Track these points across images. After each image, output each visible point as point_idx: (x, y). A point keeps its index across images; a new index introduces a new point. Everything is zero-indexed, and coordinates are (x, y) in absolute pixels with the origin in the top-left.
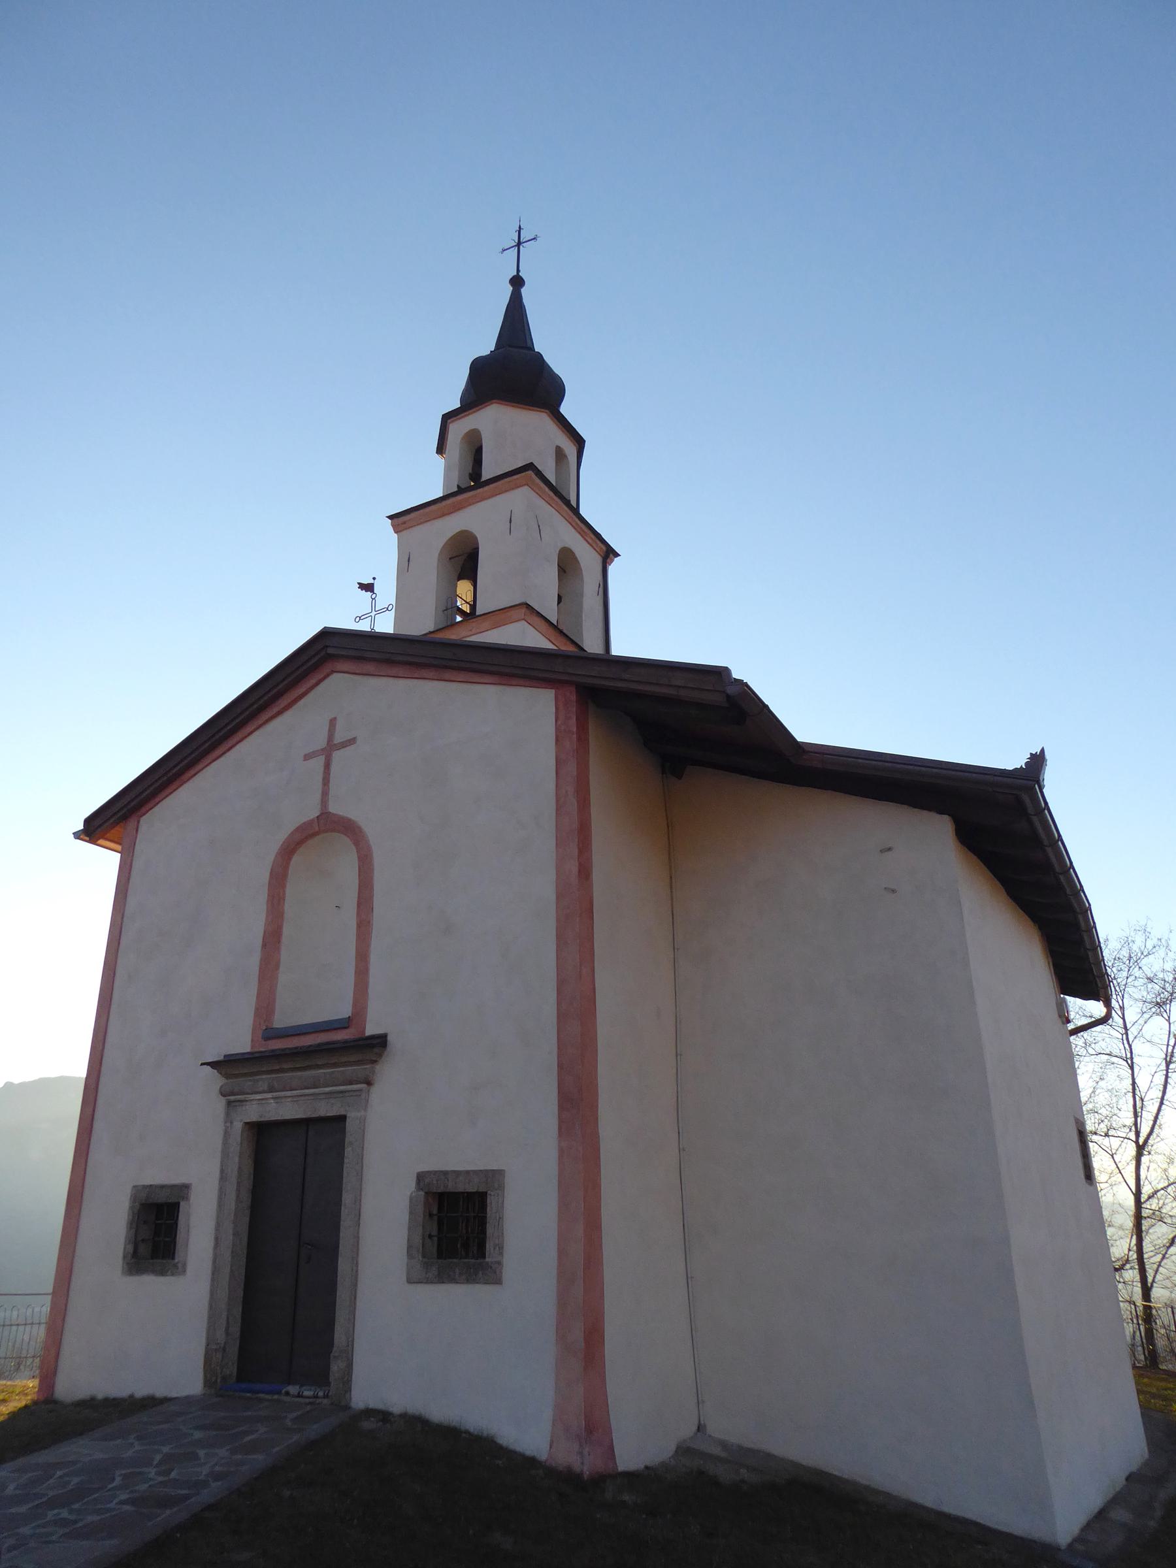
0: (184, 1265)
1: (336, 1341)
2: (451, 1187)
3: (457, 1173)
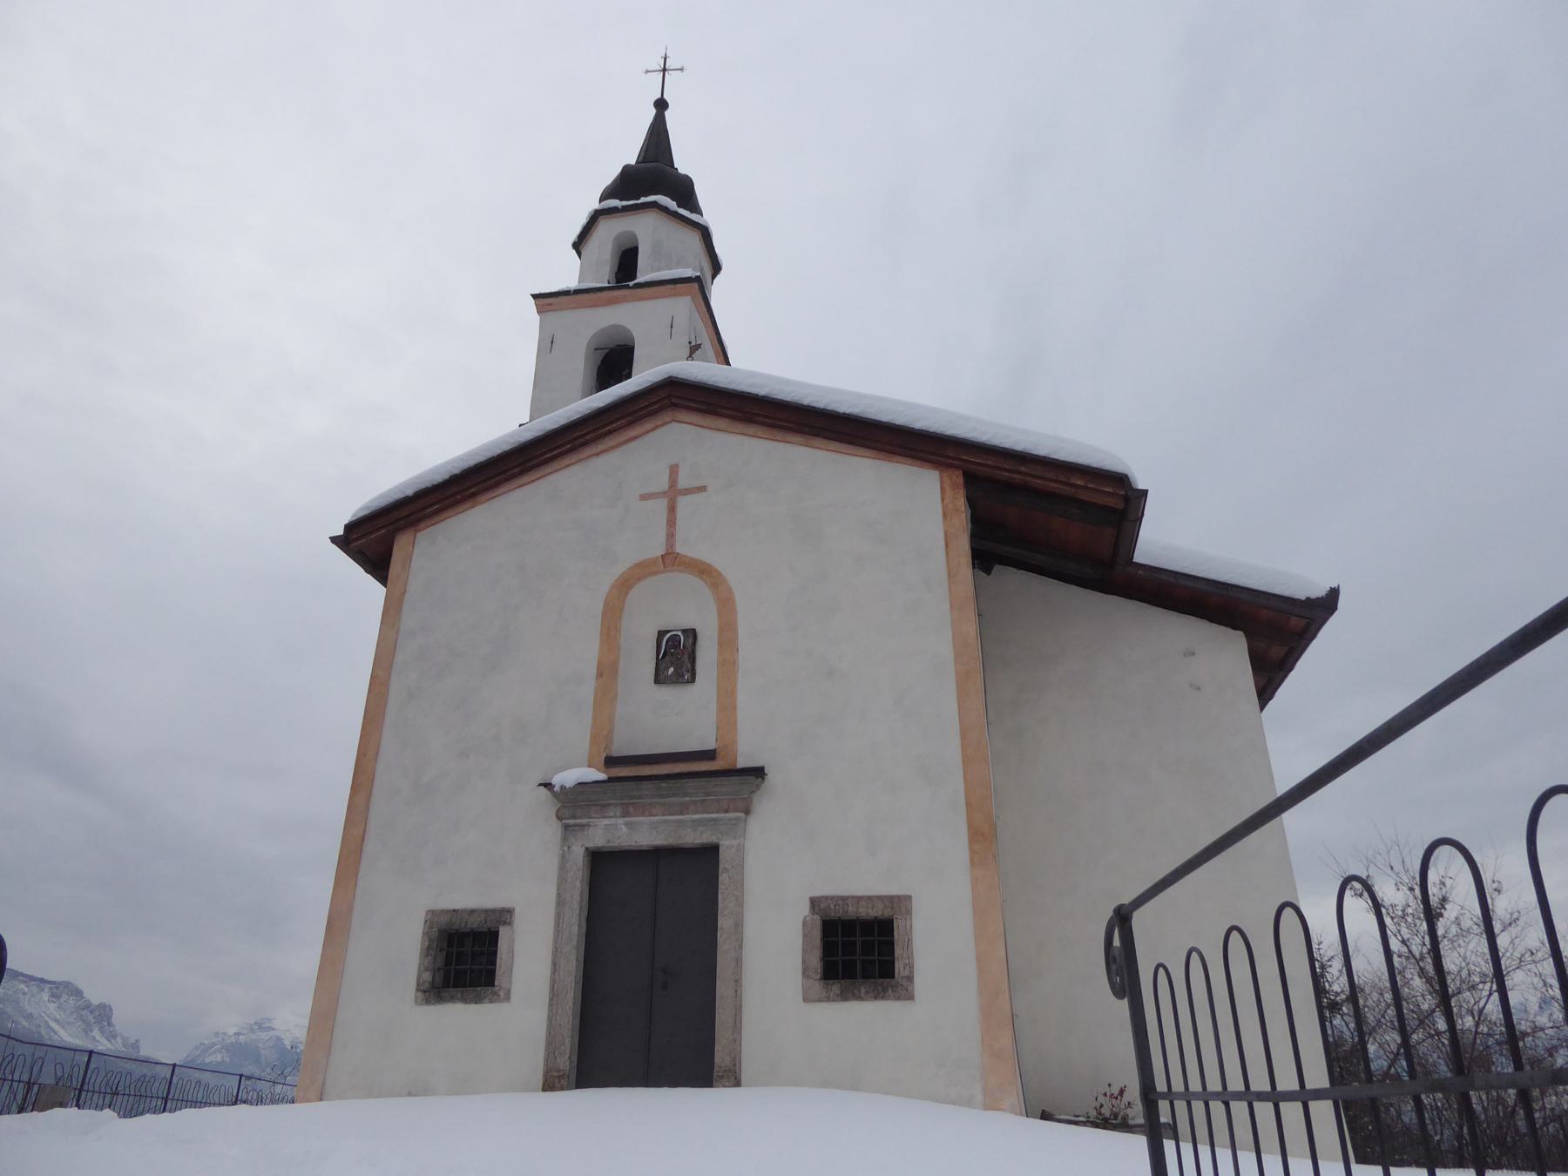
0: (508, 992)
1: (717, 1060)
2: (852, 912)
3: (859, 899)
